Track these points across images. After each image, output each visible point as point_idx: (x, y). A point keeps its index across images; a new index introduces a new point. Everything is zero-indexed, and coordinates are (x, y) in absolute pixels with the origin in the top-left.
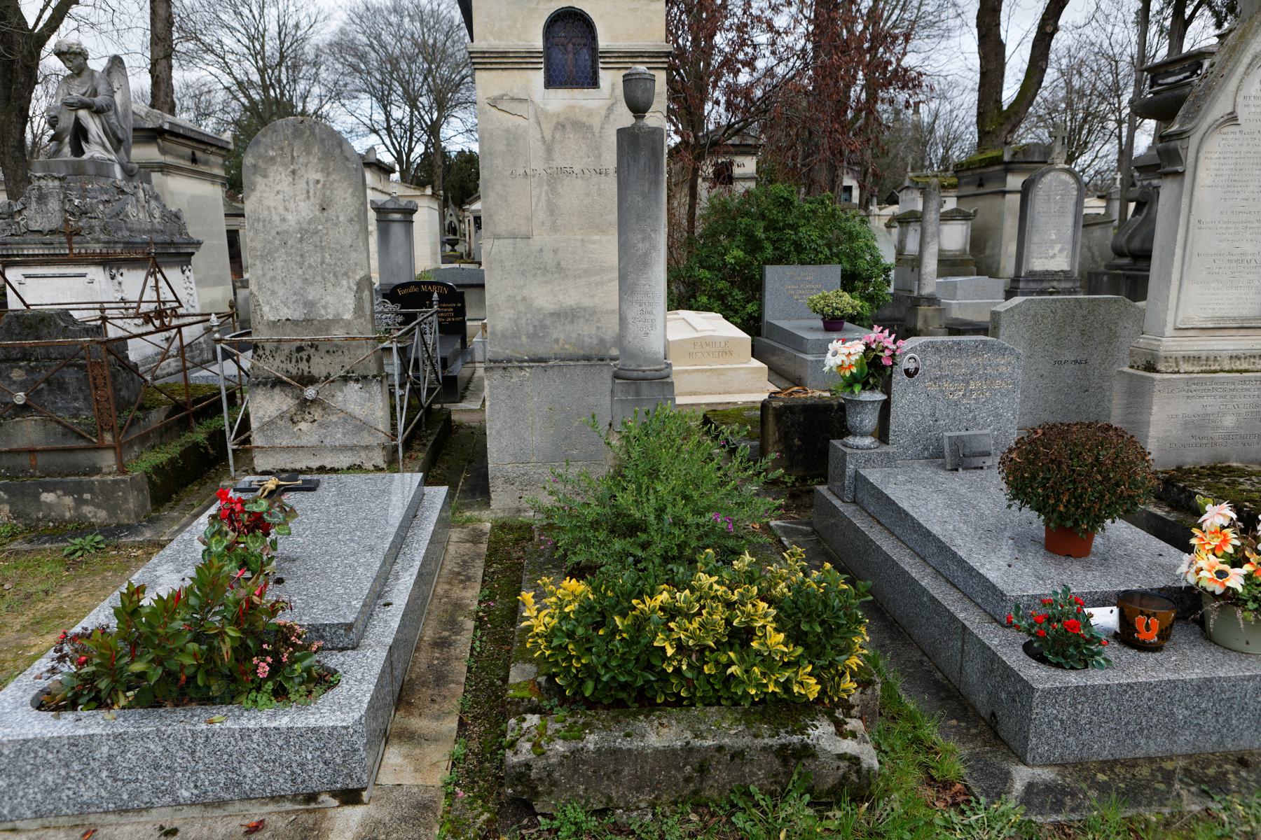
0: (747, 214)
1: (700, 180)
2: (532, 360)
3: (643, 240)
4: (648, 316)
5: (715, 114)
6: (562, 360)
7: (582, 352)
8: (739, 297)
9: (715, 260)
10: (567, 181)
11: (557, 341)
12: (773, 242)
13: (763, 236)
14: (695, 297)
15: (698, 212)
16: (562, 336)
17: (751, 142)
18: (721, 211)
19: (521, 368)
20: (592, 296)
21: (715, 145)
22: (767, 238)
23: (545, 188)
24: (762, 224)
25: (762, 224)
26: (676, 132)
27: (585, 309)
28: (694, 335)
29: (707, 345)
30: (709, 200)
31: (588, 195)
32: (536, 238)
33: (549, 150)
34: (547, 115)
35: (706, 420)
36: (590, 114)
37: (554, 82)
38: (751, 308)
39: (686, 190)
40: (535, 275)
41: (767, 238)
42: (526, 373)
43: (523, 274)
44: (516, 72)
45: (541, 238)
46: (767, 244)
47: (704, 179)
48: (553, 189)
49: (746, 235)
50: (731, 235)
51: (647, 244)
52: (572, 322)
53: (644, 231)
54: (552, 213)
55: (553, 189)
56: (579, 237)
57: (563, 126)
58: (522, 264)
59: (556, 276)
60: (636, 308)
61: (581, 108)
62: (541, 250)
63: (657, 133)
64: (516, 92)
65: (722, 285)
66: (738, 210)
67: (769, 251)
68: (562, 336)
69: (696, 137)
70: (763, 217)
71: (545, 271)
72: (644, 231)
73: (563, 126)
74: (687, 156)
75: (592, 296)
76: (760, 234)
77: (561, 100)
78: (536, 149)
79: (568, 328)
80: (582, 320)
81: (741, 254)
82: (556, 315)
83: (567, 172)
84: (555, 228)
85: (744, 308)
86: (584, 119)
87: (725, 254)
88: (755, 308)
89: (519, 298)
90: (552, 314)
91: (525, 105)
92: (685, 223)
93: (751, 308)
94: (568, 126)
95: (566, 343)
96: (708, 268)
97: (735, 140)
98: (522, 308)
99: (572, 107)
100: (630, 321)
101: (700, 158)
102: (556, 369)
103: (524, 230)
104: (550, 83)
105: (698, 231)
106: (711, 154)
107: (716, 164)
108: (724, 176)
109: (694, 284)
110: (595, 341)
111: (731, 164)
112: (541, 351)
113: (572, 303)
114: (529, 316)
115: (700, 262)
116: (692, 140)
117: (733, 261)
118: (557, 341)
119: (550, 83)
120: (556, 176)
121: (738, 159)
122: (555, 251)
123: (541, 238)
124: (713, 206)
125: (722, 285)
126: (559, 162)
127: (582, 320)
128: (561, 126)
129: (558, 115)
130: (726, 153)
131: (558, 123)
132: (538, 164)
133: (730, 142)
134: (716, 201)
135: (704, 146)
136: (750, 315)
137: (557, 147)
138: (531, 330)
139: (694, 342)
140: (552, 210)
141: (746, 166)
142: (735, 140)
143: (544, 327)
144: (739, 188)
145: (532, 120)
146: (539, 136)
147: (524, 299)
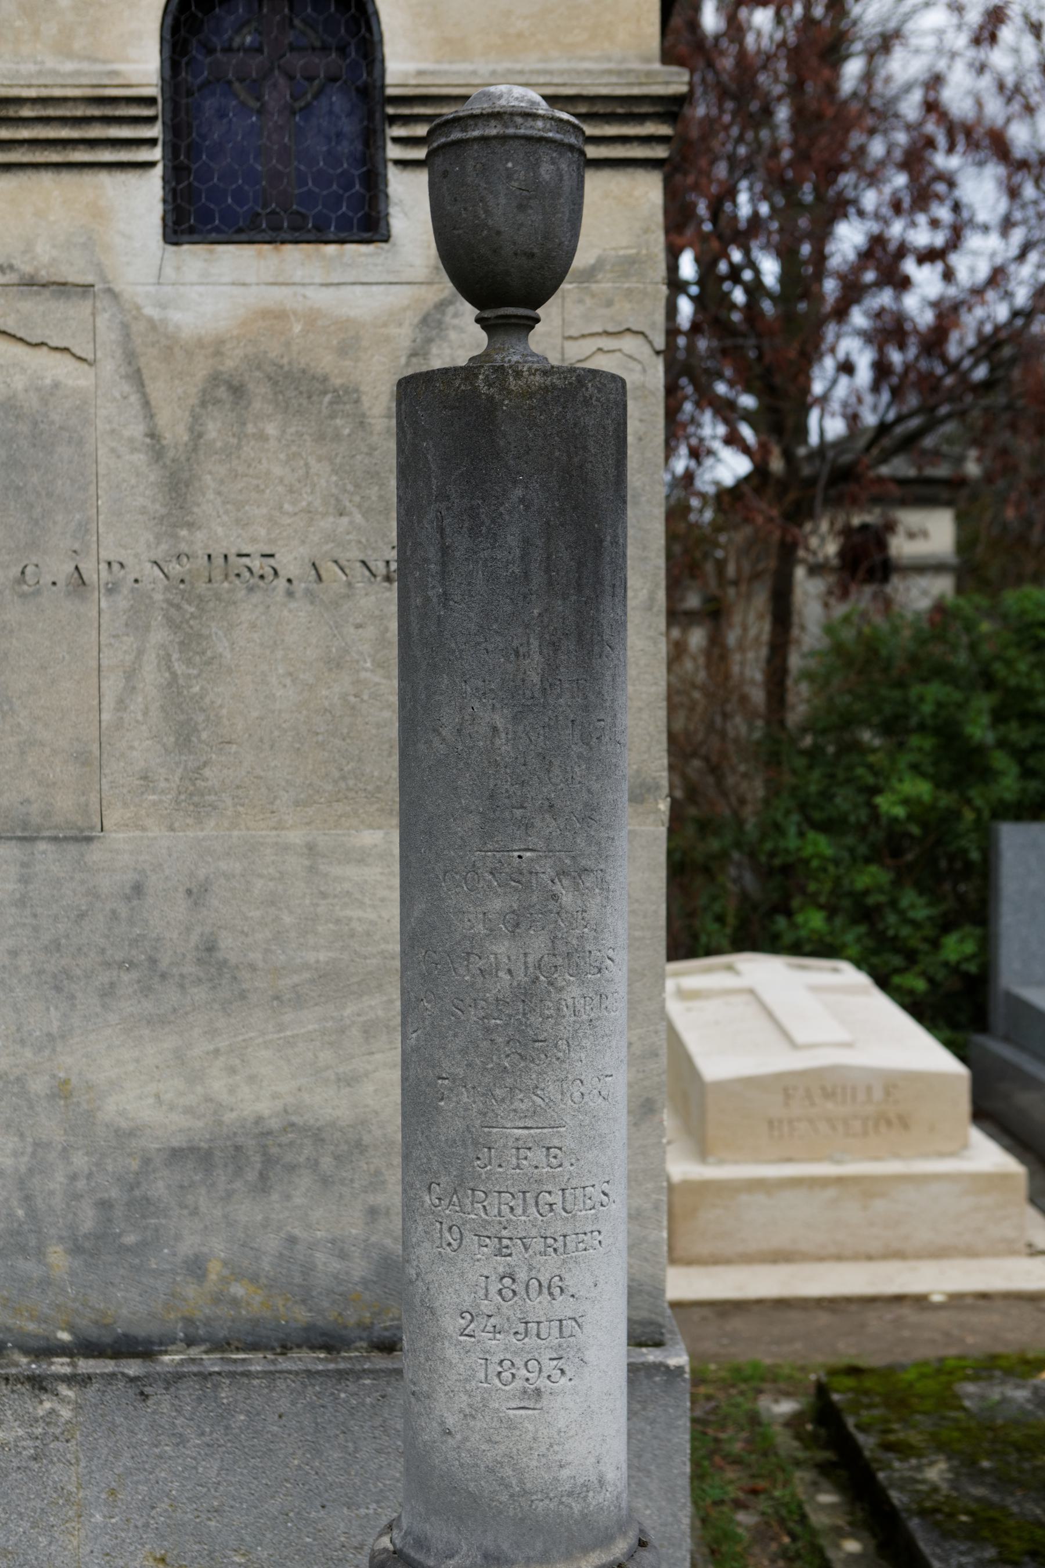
0: (942, 672)
1: (800, 572)
2: (88, 1348)
3: (517, 922)
4: (538, 1305)
5: (843, 391)
6: (220, 1345)
7: (302, 1315)
8: (921, 913)
9: (844, 800)
10: (248, 610)
11: (196, 1267)
12: (1020, 755)
13: (990, 738)
14: (789, 914)
15: (795, 661)
16: (218, 1247)
17: (942, 471)
18: (860, 660)
19: (39, 1384)
20: (350, 1081)
21: (843, 476)
22: (1002, 743)
23: (159, 635)
24: (984, 702)
25: (984, 702)
26: (732, 440)
27: (317, 1136)
28: (783, 1061)
29: (829, 1094)
30: (829, 630)
31: (336, 663)
32: (117, 838)
33: (178, 487)
34: (172, 347)
35: (824, 1419)
36: (349, 340)
37: (205, 217)
38: (956, 947)
39: (761, 600)
40: (108, 992)
41: (1002, 743)
42: (62, 1406)
43: (59, 985)
44: (47, 178)
45: (137, 840)
46: (1001, 761)
47: (815, 570)
48: (190, 641)
49: (937, 731)
50: (893, 727)
51: (538, 944)
52: (263, 1185)
53: (520, 879)
54: (185, 737)
55: (190, 641)
56: (296, 837)
57: (238, 391)
58: (55, 946)
59: (200, 994)
60: (481, 1265)
61: (312, 318)
62: (138, 889)
63: (587, 400)
64: (45, 257)
65: (871, 877)
66: (914, 660)
67: (1009, 784)
68: (218, 1247)
69: (788, 456)
70: (989, 682)
71: (153, 973)
72: (520, 879)
73: (238, 391)
74: (766, 510)
75: (350, 1081)
76: (979, 730)
77: (228, 287)
78: (120, 471)
79: (247, 1211)
80: (305, 1181)
81: (921, 789)
82: (196, 1157)
83: (256, 574)
84: (194, 800)
85: (935, 944)
86: (326, 362)
87: (876, 791)
88: (969, 948)
89: (38, 1085)
90: (175, 1155)
91: (79, 310)
92: (758, 696)
93: (956, 947)
94: (259, 391)
95: (238, 1275)
96: (827, 827)
97: (900, 467)
98: (50, 1127)
99: (279, 315)
100: (451, 1324)
101: (799, 513)
102: (188, 1391)
103: (65, 804)
104: (188, 220)
105: (798, 711)
106: (835, 502)
107: (847, 532)
108: (866, 561)
109: (786, 870)
110: (359, 1269)
111: (890, 527)
112: (128, 1306)
113: (264, 1107)
114: (80, 1161)
115: (803, 807)
116: (777, 464)
117: (900, 811)
118: (196, 1267)
119: (188, 220)
120: (199, 593)
121: (910, 518)
122: (197, 894)
123: (137, 840)
124: (838, 649)
125: (871, 877)
126: (218, 531)
127: (305, 1181)
128: (228, 390)
129: (218, 347)
130: (877, 500)
131: (215, 379)
132: (128, 541)
133: (884, 470)
134: (848, 634)
135: (811, 482)
136: (954, 969)
137: (211, 474)
138: (88, 1220)
139: (785, 1085)
140: (186, 727)
141: (930, 534)
142: (900, 467)
143: (143, 1207)
144: (920, 595)
145: (109, 366)
146: (137, 430)
147: (62, 1091)
